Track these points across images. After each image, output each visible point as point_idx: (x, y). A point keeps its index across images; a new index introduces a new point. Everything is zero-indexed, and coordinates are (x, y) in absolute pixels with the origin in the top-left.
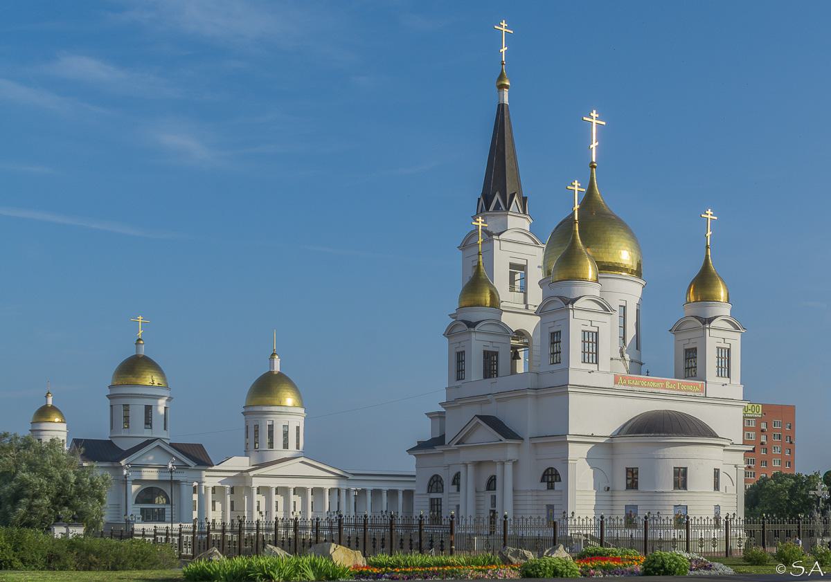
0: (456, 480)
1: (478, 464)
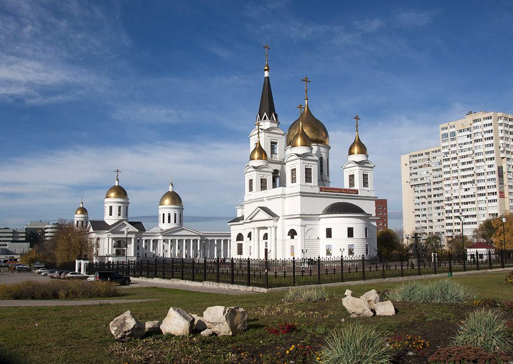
0: (249, 235)
1: (260, 228)
